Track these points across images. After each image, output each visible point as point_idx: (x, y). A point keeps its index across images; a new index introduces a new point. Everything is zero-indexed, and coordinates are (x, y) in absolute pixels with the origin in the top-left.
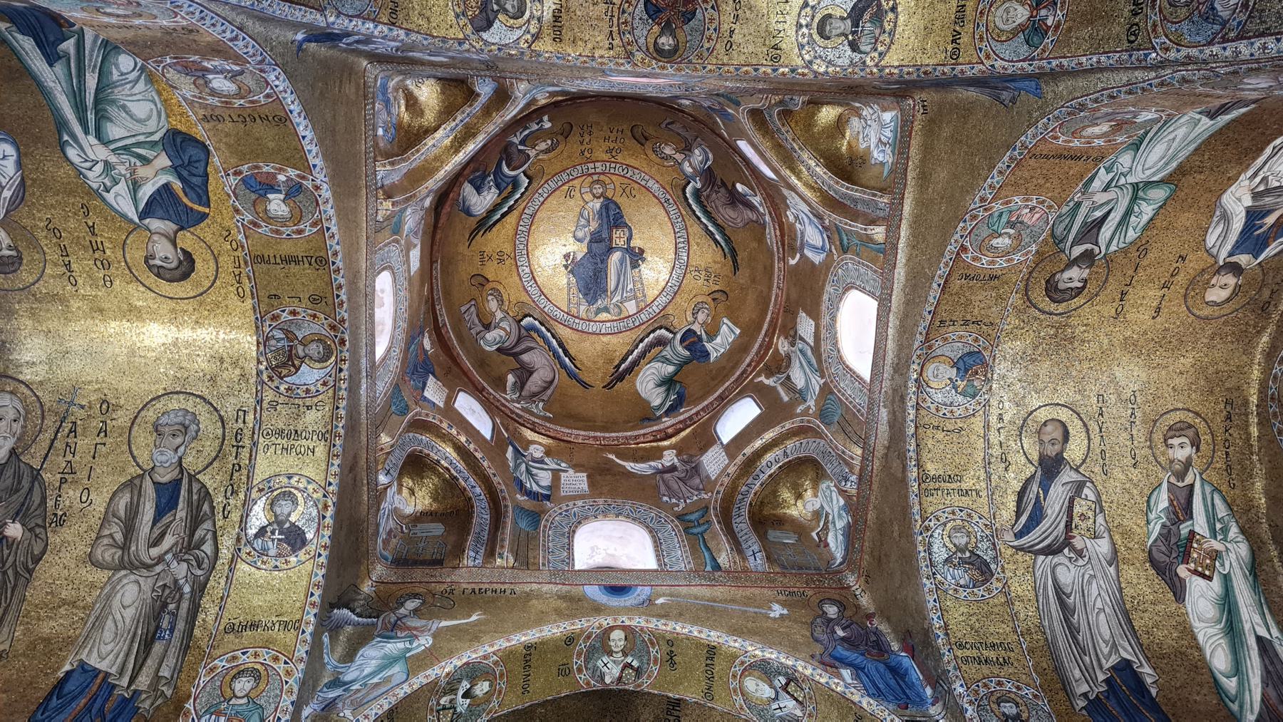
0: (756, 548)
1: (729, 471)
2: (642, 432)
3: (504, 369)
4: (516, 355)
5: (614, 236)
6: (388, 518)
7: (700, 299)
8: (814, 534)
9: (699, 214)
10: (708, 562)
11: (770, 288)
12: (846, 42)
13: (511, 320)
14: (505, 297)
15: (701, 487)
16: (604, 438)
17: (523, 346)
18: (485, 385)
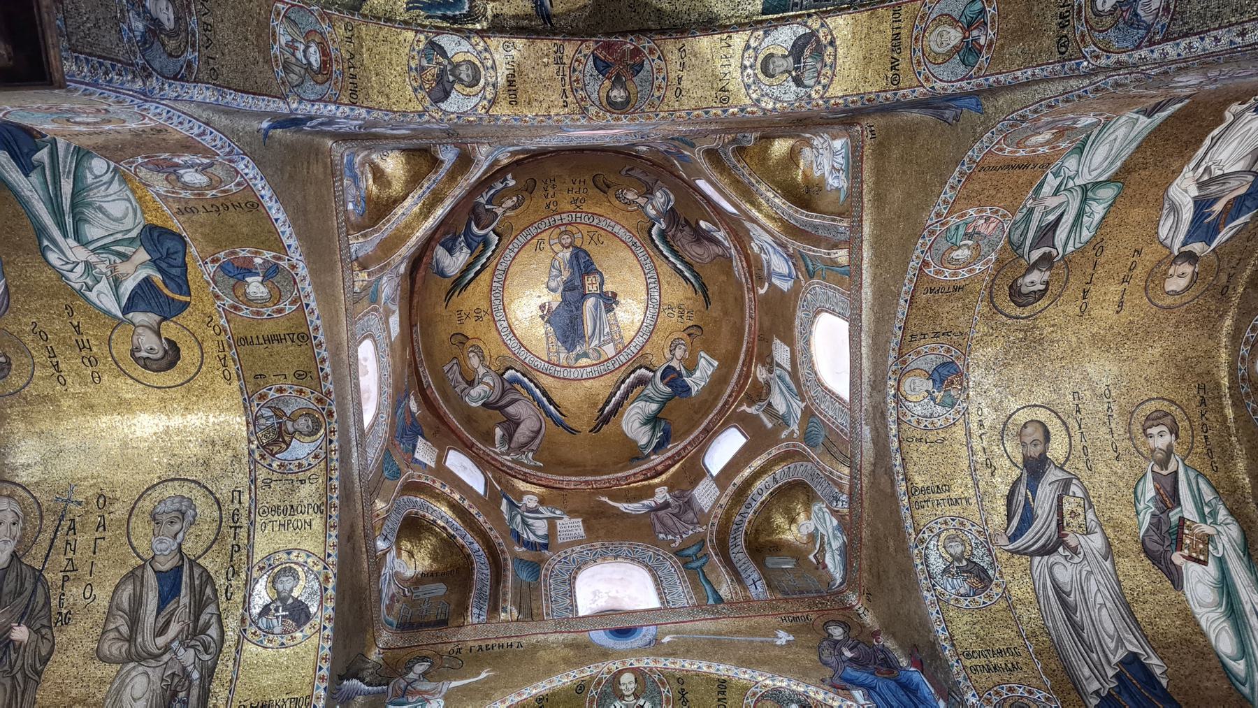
0: (755, 576)
2: (632, 471)
4: (501, 409)
7: (675, 336)
8: (811, 557)
9: (666, 254)
12: (790, 78)
13: (493, 374)
14: (486, 353)
15: (695, 520)
16: (596, 482)
17: (507, 399)
18: (474, 441)
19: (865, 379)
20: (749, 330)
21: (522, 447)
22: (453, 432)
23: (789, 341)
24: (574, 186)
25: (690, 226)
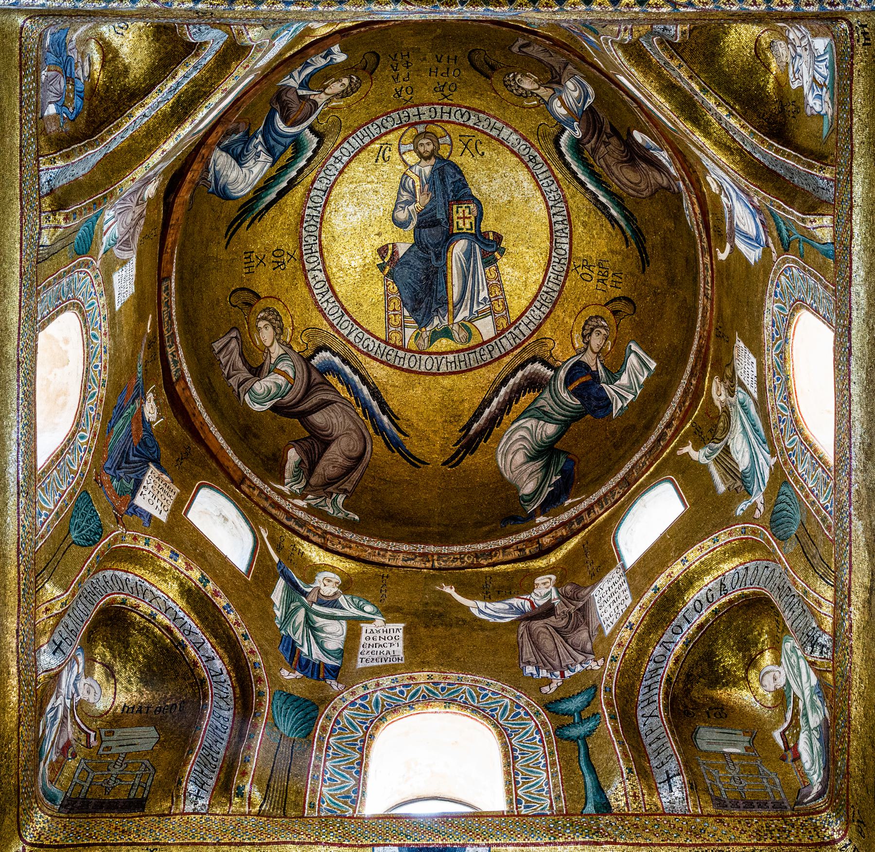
0: (672, 766)
1: (632, 619)
2: (502, 542)
3: (282, 442)
4: (303, 416)
5: (455, 217)
6: (63, 723)
7: (592, 311)
8: (777, 735)
9: (583, 178)
10: (590, 795)
11: (696, 295)
13: (295, 357)
14: (286, 321)
15: (589, 647)
16: (440, 555)
17: (314, 400)
18: (247, 471)
19: (856, 439)
20: (703, 317)
21: (328, 486)
22: (214, 457)
23: (757, 349)
24: (440, 65)
25: (619, 137)
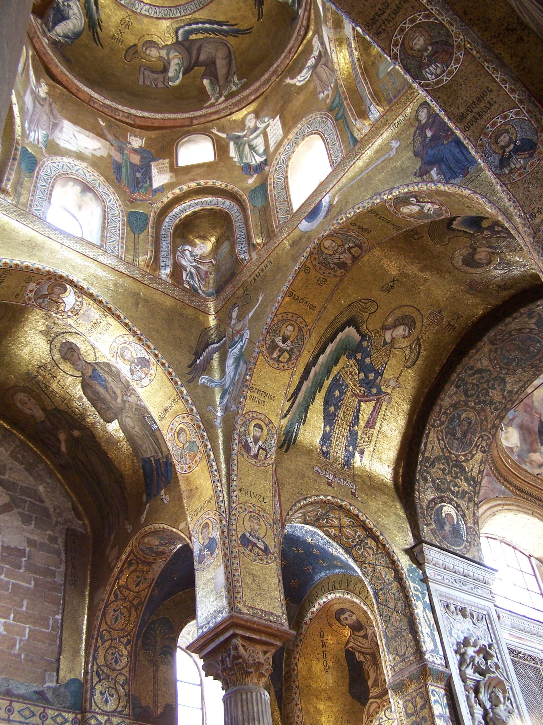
17: (195, 52)
21: (228, 80)
